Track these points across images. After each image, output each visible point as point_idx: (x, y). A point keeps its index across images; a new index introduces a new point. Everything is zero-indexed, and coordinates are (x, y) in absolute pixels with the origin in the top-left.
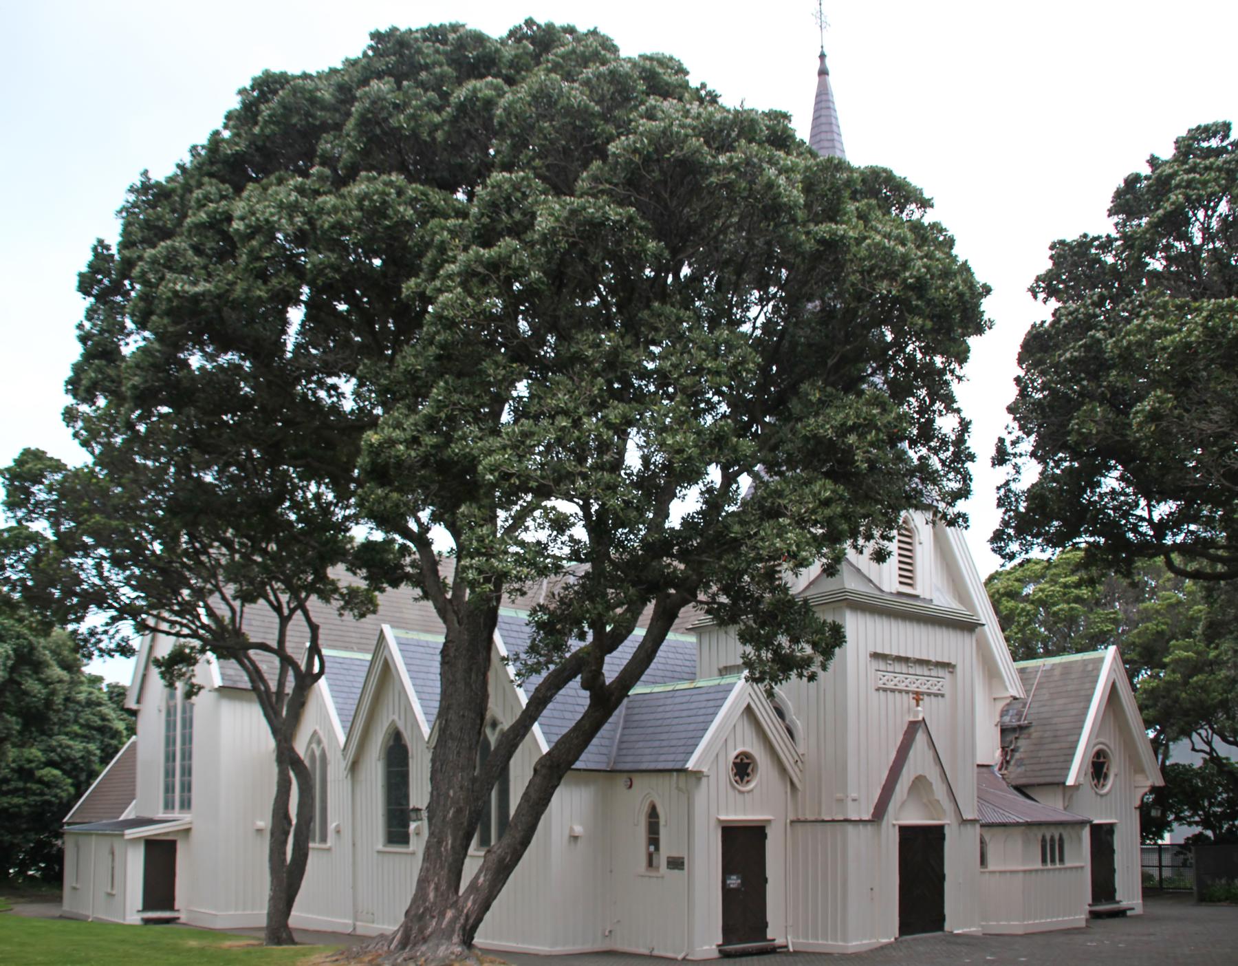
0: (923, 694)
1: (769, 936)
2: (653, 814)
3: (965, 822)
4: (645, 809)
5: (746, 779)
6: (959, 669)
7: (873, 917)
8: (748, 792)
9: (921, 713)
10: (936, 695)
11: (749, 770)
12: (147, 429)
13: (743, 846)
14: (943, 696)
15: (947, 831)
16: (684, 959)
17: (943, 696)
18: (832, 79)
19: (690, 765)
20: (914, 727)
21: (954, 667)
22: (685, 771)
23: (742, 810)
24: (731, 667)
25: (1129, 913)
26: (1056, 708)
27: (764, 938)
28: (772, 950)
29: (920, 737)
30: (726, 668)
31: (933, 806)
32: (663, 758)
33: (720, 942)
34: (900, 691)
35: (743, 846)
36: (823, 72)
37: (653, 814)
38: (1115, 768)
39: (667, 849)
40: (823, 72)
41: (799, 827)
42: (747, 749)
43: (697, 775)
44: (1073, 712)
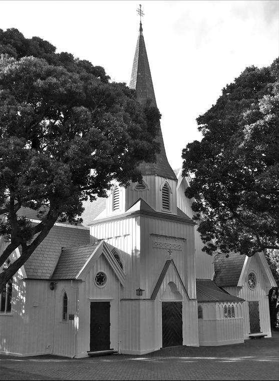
0: (173, 250)
1: (111, 348)
2: (65, 297)
3: (190, 300)
4: (63, 295)
5: (102, 283)
6: (187, 240)
7: (152, 339)
8: (102, 288)
9: (172, 256)
10: (160, 248)
11: (103, 280)
12: (28, 150)
13: (100, 313)
14: (181, 251)
15: (183, 304)
16: (74, 358)
17: (181, 251)
18: (144, 32)
19: (77, 277)
20: (168, 263)
21: (186, 240)
22: (74, 280)
23: (101, 295)
24: (154, 234)
25: (265, 337)
26: (234, 257)
27: (109, 349)
28: (112, 354)
29: (171, 266)
30: (152, 234)
31: (177, 293)
32: (69, 274)
33: (89, 350)
34: (163, 249)
35: (100, 313)
36: (141, 30)
37: (65, 297)
38: (258, 277)
39: (69, 312)
40: (141, 30)
41: (124, 303)
42: (102, 271)
43: (79, 281)
44: (240, 259)
